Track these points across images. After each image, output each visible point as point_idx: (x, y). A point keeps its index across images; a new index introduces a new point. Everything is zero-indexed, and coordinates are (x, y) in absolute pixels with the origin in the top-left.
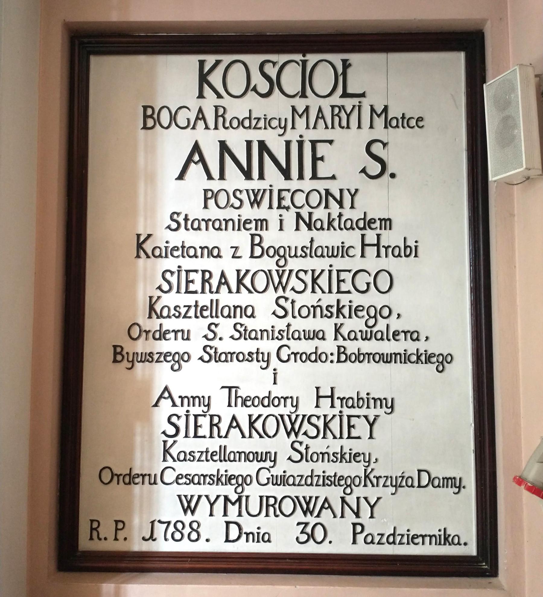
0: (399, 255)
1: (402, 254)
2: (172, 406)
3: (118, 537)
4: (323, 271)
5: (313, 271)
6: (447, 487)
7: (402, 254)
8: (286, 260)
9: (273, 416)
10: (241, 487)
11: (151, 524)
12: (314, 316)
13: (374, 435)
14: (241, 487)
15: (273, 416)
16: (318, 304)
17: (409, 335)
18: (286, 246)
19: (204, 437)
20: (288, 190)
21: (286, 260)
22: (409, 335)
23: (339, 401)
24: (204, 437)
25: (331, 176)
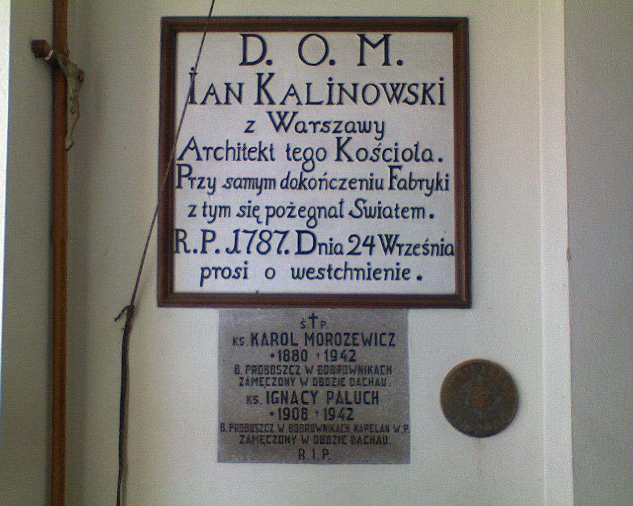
0: (405, 188)
1: (407, 186)
2: (269, 104)
3: (207, 249)
4: (433, 85)
5: (425, 85)
6: (270, 188)
7: (407, 186)
8: (313, 163)
9: (374, 85)
10: (310, 162)
11: (234, 234)
12: (320, 188)
13: (366, 61)
14: (310, 162)
15: (374, 85)
16: (325, 177)
17: (219, 272)
18: (355, 121)
19: (245, 231)
20: (301, 173)
21: (313, 163)
22: (219, 272)
23: (312, 125)
24: (245, 231)
25: (234, 235)
